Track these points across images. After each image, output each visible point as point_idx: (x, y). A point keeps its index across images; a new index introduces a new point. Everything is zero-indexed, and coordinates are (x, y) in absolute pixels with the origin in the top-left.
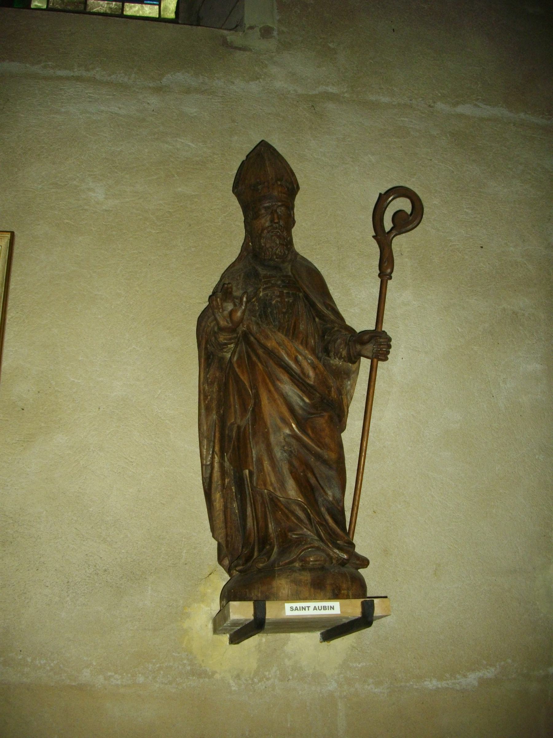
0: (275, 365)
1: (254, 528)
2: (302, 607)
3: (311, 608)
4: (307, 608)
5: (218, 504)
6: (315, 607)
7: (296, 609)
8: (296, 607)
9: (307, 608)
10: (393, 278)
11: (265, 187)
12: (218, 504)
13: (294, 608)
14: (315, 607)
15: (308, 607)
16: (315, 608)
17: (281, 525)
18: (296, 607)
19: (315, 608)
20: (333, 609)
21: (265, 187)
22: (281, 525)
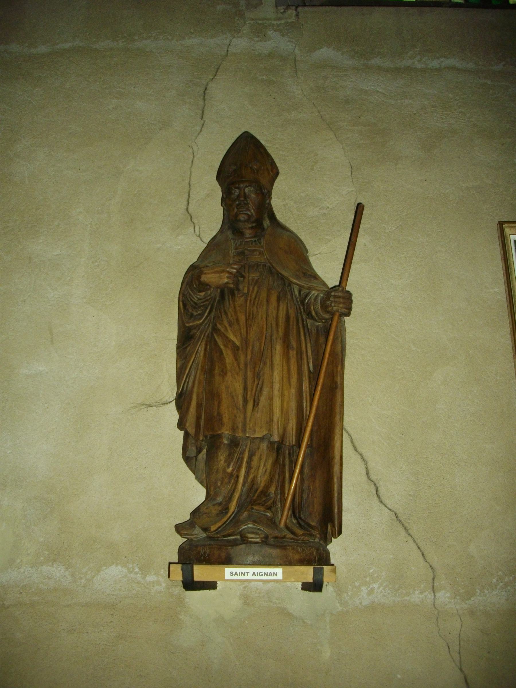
0: (256, 326)
1: (293, 431)
2: (242, 573)
3: (250, 574)
4: (246, 574)
5: (183, 289)
6: (254, 573)
7: (236, 574)
8: (236, 572)
9: (246, 574)
10: (351, 315)
11: (246, 170)
12: (183, 289)
13: (234, 574)
14: (254, 573)
15: (248, 573)
16: (254, 574)
17: (268, 490)
18: (236, 572)
19: (254, 574)
20: (276, 575)
21: (246, 170)
22: (268, 490)
